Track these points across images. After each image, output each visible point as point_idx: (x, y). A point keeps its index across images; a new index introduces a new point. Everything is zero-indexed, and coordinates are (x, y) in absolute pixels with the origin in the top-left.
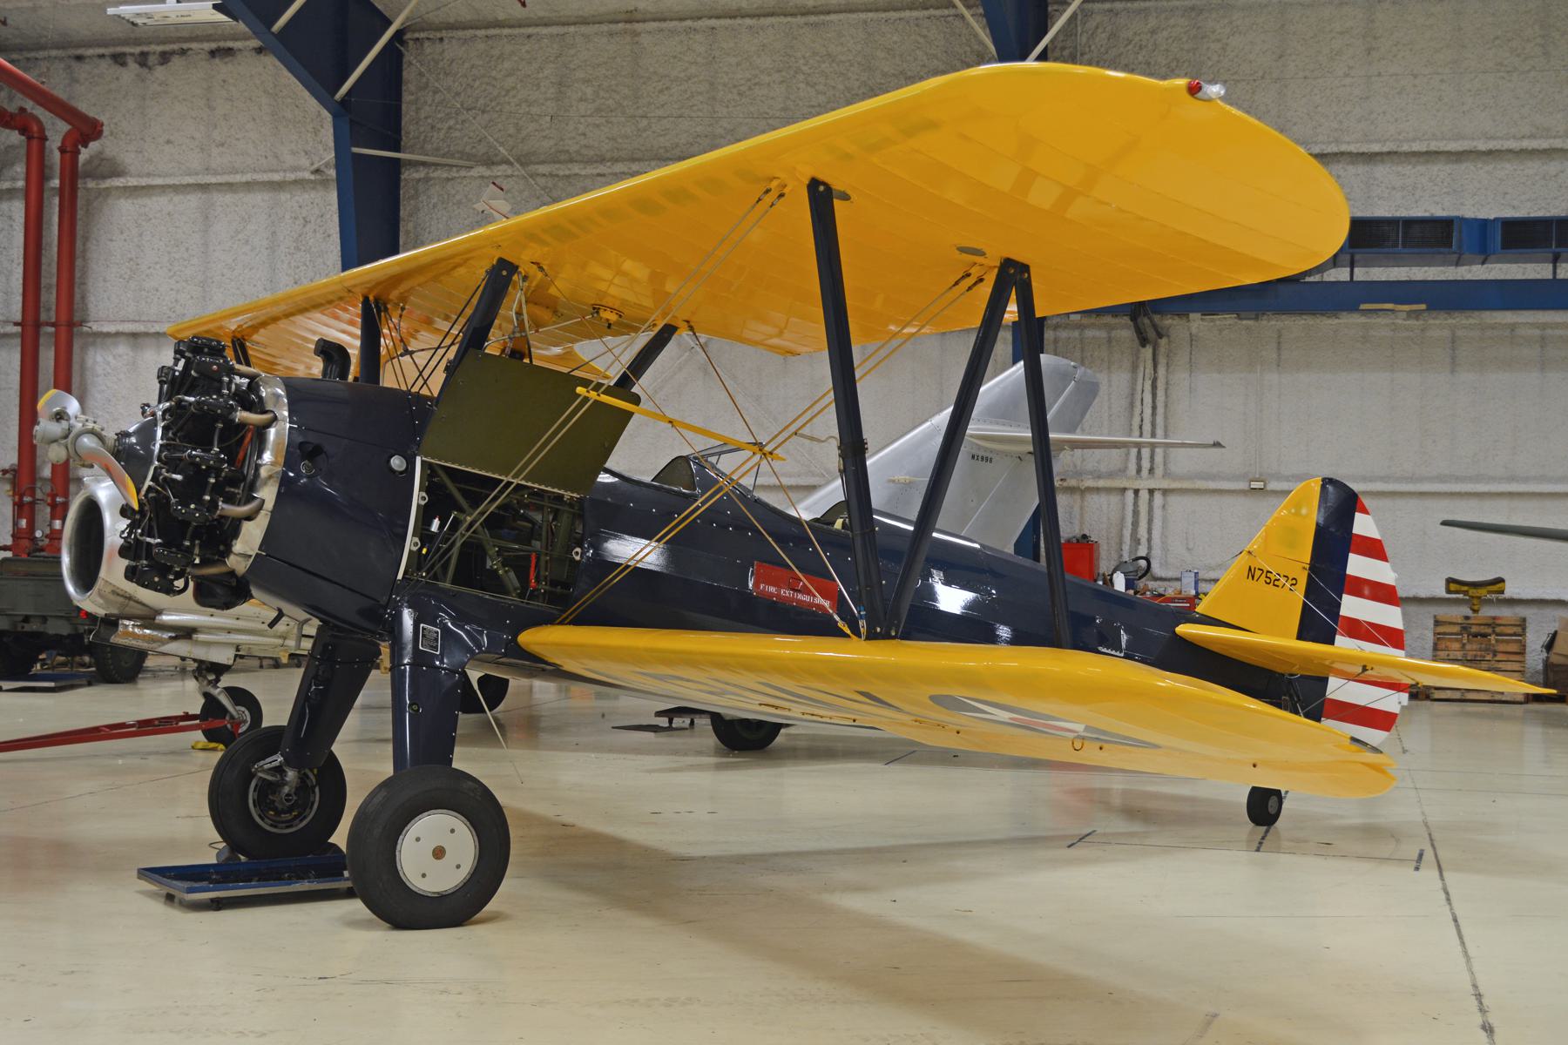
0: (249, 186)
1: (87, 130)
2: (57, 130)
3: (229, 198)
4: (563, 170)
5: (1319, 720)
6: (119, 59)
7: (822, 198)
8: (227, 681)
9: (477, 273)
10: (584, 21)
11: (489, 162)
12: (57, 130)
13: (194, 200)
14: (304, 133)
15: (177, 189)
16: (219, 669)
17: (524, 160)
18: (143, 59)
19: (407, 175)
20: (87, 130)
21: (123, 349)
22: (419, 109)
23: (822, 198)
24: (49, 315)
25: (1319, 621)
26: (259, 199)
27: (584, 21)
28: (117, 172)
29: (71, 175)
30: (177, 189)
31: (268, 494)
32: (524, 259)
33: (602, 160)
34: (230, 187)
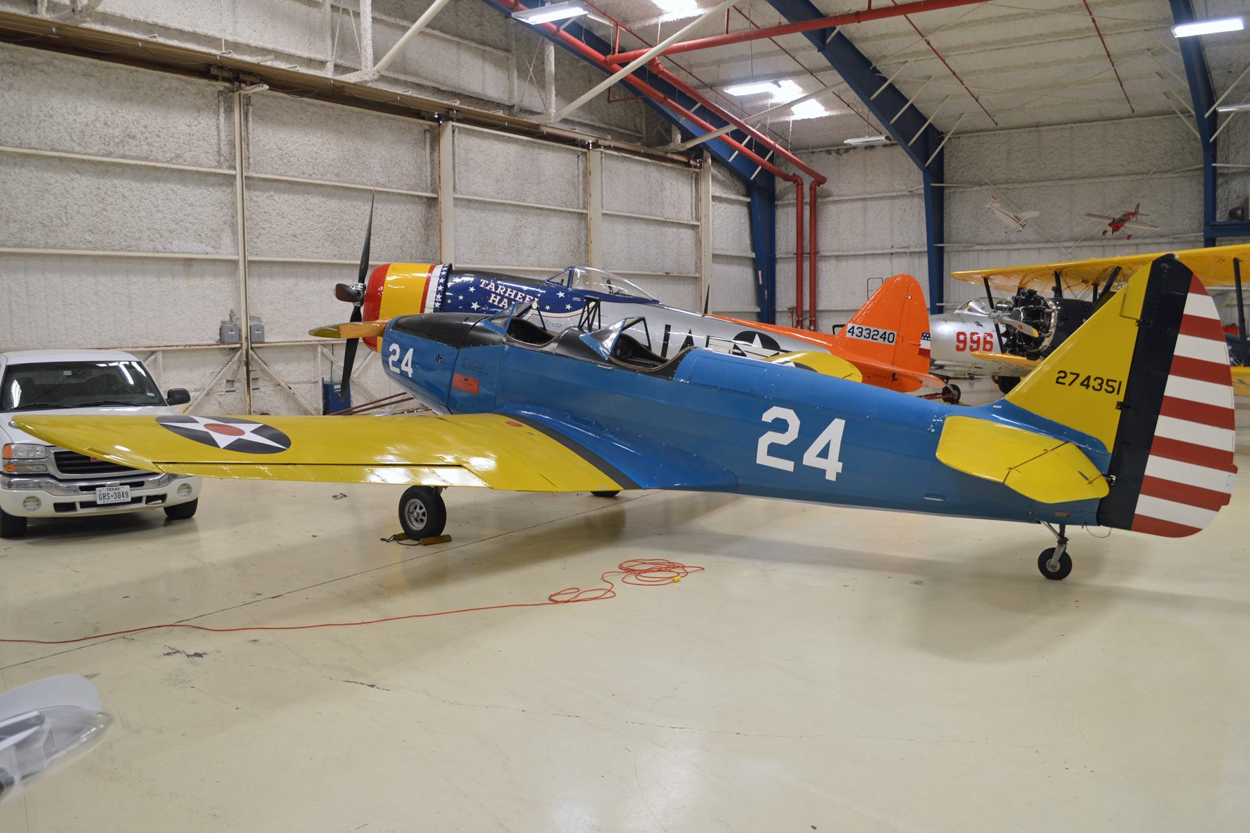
0: (882, 198)
1: (820, 180)
2: (808, 181)
3: (874, 203)
4: (1010, 186)
5: (1217, 510)
6: (829, 152)
7: (1236, 262)
8: (951, 382)
9: (1110, 271)
10: (1018, 128)
11: (980, 185)
12: (808, 181)
13: (859, 204)
14: (914, 178)
15: (853, 200)
16: (948, 378)
17: (995, 183)
18: (838, 152)
19: (946, 191)
20: (820, 180)
21: (833, 261)
22: (950, 166)
23: (1236, 262)
24: (807, 249)
25: (714, 313)
26: (886, 202)
27: (1018, 128)
28: (828, 196)
29: (814, 197)
30: (853, 200)
31: (1052, 330)
32: (1123, 267)
33: (1026, 181)
34: (874, 199)
